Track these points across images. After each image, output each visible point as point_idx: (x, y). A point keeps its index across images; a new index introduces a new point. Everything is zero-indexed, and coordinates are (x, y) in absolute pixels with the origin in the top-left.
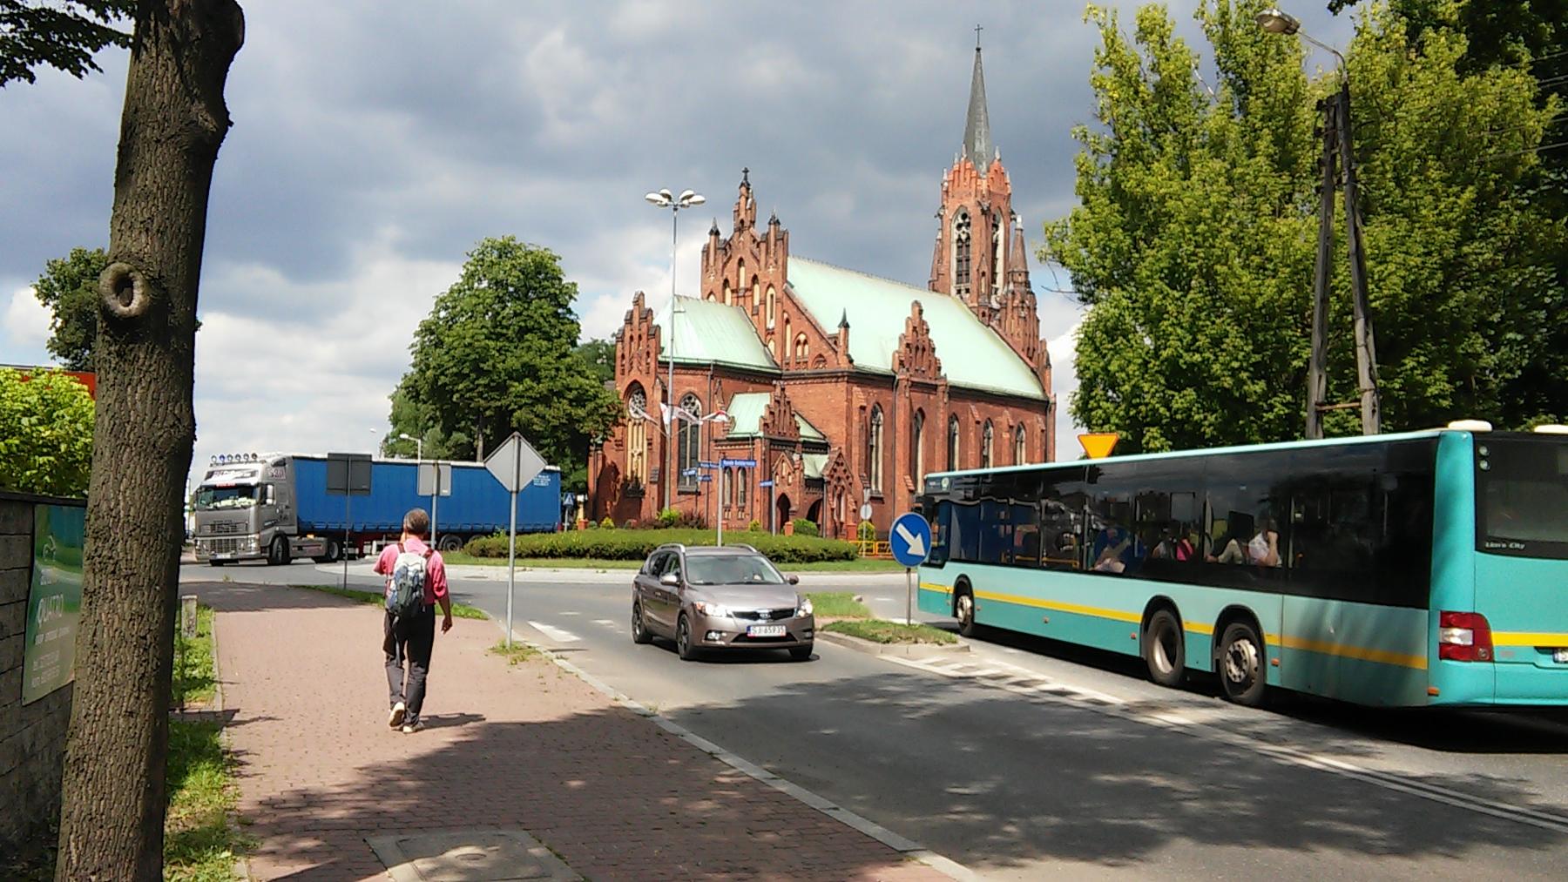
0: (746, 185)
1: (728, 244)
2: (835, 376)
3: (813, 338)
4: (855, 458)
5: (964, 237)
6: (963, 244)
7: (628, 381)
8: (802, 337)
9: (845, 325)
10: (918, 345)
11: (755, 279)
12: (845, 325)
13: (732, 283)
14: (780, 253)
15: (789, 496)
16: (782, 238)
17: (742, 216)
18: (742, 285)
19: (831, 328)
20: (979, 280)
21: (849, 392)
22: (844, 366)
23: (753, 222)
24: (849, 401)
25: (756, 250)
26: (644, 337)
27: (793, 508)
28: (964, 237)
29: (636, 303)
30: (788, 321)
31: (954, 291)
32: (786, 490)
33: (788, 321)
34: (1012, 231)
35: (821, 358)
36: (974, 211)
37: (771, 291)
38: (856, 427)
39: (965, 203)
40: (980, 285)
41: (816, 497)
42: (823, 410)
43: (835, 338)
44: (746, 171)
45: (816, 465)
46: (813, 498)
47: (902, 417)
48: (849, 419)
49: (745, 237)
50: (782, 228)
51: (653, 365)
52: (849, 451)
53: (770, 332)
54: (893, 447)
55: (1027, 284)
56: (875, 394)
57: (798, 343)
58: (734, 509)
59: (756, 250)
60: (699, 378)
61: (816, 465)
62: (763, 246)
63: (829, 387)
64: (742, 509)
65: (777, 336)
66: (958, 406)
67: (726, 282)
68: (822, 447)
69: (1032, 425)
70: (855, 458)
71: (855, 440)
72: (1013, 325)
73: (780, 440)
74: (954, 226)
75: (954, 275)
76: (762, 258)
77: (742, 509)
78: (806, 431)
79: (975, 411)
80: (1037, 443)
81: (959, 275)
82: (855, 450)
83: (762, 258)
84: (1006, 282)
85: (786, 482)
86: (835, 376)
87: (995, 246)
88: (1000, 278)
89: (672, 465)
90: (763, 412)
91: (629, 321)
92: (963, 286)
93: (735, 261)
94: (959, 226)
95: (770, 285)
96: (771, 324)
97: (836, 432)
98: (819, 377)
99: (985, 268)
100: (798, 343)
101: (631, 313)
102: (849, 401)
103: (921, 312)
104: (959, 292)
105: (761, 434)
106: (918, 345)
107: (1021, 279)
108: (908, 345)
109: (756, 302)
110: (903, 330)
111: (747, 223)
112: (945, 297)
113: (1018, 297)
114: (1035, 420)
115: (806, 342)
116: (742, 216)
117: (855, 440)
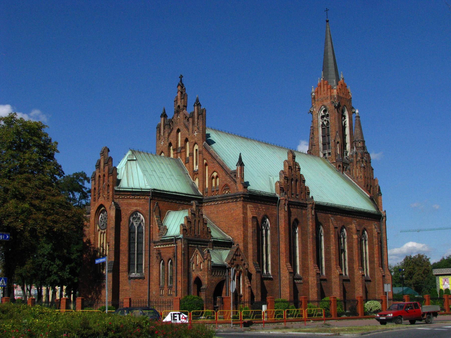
0: (181, 85)
1: (171, 121)
2: (235, 198)
3: (222, 174)
4: (250, 252)
5: (325, 123)
6: (325, 128)
7: (97, 205)
8: (215, 174)
9: (241, 163)
10: (292, 178)
11: (187, 140)
12: (241, 163)
13: (174, 144)
14: (201, 123)
15: (202, 278)
16: (202, 114)
17: (179, 103)
18: (179, 146)
19: (232, 166)
20: (335, 146)
21: (244, 208)
22: (241, 189)
23: (185, 106)
24: (245, 213)
25: (186, 123)
26: (107, 175)
27: (204, 287)
28: (325, 123)
29: (102, 154)
30: (206, 165)
31: (321, 155)
32: (199, 274)
33: (206, 165)
34: (354, 119)
35: (226, 187)
36: (331, 108)
37: (196, 147)
38: (250, 230)
39: (325, 103)
40: (336, 150)
41: (220, 278)
42: (226, 222)
43: (235, 172)
44: (181, 77)
45: (221, 256)
46: (216, 280)
47: (282, 224)
48: (245, 225)
49: (181, 116)
50: (202, 107)
51: (111, 193)
52: (246, 247)
53: (195, 174)
54: (279, 245)
55: (364, 148)
56: (262, 209)
57: (213, 178)
58: (166, 288)
59: (186, 123)
60: (142, 201)
61: (221, 256)
62: (191, 120)
63: (232, 205)
64: (171, 288)
65: (200, 175)
66: (321, 216)
67: (170, 145)
68: (226, 244)
69: (372, 230)
70: (250, 252)
71: (250, 240)
72: (358, 172)
73: (196, 238)
74: (320, 117)
75: (321, 146)
76: (191, 127)
77: (171, 288)
78: (215, 234)
79: (333, 221)
80: (375, 241)
81: (324, 144)
82: (250, 246)
83: (191, 127)
84: (352, 147)
85: (199, 266)
86: (235, 198)
87: (344, 128)
88: (348, 146)
89: (124, 259)
90: (183, 221)
91: (98, 166)
92: (327, 152)
93: (175, 131)
94: (323, 117)
95: (195, 143)
96: (196, 168)
97: (235, 235)
98: (225, 199)
99: (339, 140)
100: (213, 178)
101: (99, 162)
102: (245, 213)
103: (294, 157)
104: (324, 155)
105: (181, 236)
106: (292, 178)
107: (360, 145)
108: (285, 177)
109: (188, 156)
110: (282, 168)
111: (181, 107)
112: (318, 159)
113: (359, 155)
114: (373, 226)
115: (217, 177)
116: (179, 103)
117: (250, 240)
